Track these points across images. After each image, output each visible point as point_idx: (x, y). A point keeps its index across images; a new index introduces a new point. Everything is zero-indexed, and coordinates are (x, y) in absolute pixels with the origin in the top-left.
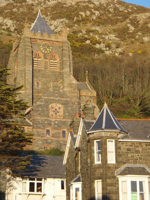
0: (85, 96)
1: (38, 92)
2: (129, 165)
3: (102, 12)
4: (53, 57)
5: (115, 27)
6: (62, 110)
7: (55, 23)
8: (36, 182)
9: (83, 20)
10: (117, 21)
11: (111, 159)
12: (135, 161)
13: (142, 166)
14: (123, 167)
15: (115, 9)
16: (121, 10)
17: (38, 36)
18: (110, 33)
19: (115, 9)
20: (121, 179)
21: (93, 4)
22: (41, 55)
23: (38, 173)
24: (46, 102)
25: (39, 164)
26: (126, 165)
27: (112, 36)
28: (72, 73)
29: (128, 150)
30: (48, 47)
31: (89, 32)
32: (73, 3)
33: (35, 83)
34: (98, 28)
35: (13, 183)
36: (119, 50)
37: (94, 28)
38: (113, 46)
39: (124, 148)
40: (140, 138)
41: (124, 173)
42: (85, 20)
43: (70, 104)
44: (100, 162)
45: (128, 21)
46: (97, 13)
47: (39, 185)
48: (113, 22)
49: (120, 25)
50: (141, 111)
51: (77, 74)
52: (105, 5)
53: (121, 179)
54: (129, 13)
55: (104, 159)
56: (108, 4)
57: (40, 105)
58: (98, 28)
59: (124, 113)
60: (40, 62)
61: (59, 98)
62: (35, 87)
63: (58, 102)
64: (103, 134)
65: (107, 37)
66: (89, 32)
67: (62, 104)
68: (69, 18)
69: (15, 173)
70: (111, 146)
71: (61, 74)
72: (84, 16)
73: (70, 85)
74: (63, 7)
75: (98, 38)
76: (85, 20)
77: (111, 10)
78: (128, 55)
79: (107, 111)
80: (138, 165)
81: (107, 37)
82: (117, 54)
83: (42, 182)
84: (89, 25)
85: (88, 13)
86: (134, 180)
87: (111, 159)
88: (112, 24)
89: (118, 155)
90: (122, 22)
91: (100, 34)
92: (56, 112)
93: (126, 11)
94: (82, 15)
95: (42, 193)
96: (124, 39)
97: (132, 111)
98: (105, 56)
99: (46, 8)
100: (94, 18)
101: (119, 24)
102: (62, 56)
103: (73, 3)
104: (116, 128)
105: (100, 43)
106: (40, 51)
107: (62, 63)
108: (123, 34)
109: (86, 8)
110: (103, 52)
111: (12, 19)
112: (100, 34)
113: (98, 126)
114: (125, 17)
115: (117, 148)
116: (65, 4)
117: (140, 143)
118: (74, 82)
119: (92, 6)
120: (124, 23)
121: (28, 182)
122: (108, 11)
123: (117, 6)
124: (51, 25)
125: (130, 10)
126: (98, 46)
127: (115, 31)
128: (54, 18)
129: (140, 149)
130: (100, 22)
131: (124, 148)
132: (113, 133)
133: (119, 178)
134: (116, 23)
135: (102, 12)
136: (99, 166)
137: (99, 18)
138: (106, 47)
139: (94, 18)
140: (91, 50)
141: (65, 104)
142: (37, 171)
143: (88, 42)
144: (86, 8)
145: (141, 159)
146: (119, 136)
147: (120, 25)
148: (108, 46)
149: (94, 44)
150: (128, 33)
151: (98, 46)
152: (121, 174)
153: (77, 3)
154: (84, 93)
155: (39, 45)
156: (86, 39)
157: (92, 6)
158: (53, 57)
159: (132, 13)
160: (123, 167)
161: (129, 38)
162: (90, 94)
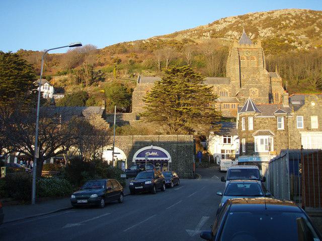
0: (275, 81)
1: (244, 81)
2: (261, 130)
3: (297, 20)
4: (253, 59)
5: (306, 30)
6: (257, 92)
7: (265, 31)
8: (227, 138)
9: (284, 27)
10: (308, 25)
11: (251, 128)
12: (264, 128)
13: (267, 130)
14: (257, 132)
15: (307, 17)
16: (311, 17)
17: (243, 46)
18: (302, 34)
19: (307, 17)
20: (256, 137)
21: (291, 15)
22: (245, 58)
23: (229, 133)
24: (247, 87)
25: (232, 128)
26: (259, 131)
27: (304, 36)
28: (265, 67)
29: (260, 122)
30: (249, 52)
31: (287, 35)
32: (278, 16)
33: (242, 76)
34: (293, 32)
35: (215, 138)
36: (308, 45)
37: (291, 32)
38: (304, 43)
39: (258, 121)
40: (267, 115)
41: (257, 135)
42: (286, 27)
43: (263, 88)
44: (244, 129)
45: (315, 24)
46: (294, 21)
47: (229, 140)
48: (304, 26)
49: (310, 28)
50: (317, 87)
51: (270, 67)
52: (300, 15)
53: (256, 137)
54: (317, 19)
55: (247, 128)
56: (301, 14)
57: (244, 90)
58: (293, 32)
59: (306, 89)
60: (244, 63)
61: (255, 85)
62: (242, 78)
63: (255, 87)
64: (246, 114)
65: (299, 37)
66: (287, 35)
67: (258, 88)
68: (275, 26)
69: (216, 133)
70: (251, 120)
71: (258, 68)
72: (285, 24)
73: (264, 75)
74: (271, 20)
75: (293, 39)
76: (286, 27)
77: (304, 18)
78: (314, 48)
79: (250, 101)
80: (265, 130)
81: (299, 37)
82: (306, 48)
83: (231, 138)
84: (287, 30)
85: (288, 22)
86: (262, 138)
87: (251, 128)
88: (304, 28)
89: (254, 125)
90: (311, 25)
91: (295, 36)
92: (254, 93)
93: (314, 17)
94: (283, 24)
95: (231, 144)
96: (311, 37)
97: (310, 87)
98: (298, 50)
99: (260, 21)
100: (292, 24)
101: (309, 27)
102: (258, 57)
103: (278, 16)
104: (253, 110)
105: (294, 42)
106: (244, 55)
107: (258, 62)
108: (311, 34)
109: (287, 18)
110: (296, 48)
111: (237, 31)
112: (295, 36)
113: (244, 110)
114: (313, 22)
115: (254, 121)
116: (272, 17)
117: (267, 118)
118: (267, 73)
119: (290, 16)
120: (313, 26)
121: (223, 138)
122: (302, 19)
123: (308, 14)
124: (262, 32)
125: (317, 16)
126: (293, 44)
127: (305, 32)
128: (264, 28)
129: (267, 121)
130: (296, 27)
131: (258, 121)
132: (252, 113)
133: (302, 135)
134: (307, 27)
135: (297, 20)
136: (244, 132)
137: (295, 24)
138: (298, 44)
139: (292, 24)
140: (287, 47)
141: (260, 88)
142: (229, 131)
143: (286, 42)
144: (287, 18)
145: (267, 126)
146: (255, 115)
147: (310, 28)
148: (301, 43)
149: (291, 43)
150: (315, 33)
151: (293, 44)
152: (256, 135)
153: (280, 16)
154: (273, 79)
155: (243, 52)
156: (285, 40)
157: (290, 16)
158: (253, 59)
159: (319, 18)
160: (257, 132)
161: (315, 36)
162: (277, 80)
